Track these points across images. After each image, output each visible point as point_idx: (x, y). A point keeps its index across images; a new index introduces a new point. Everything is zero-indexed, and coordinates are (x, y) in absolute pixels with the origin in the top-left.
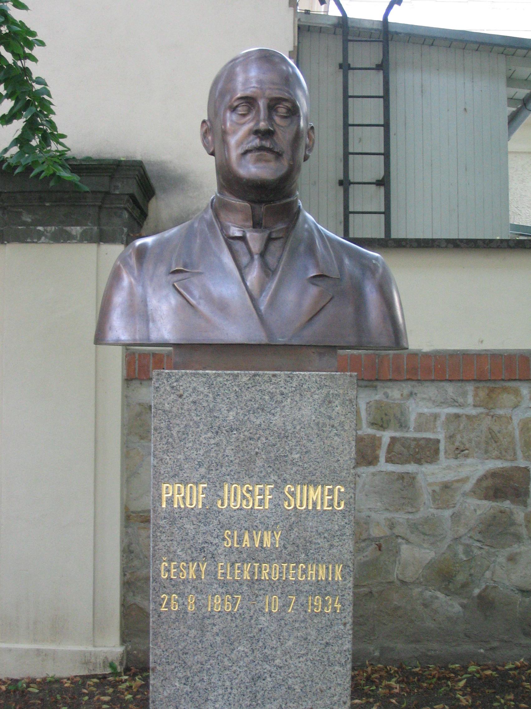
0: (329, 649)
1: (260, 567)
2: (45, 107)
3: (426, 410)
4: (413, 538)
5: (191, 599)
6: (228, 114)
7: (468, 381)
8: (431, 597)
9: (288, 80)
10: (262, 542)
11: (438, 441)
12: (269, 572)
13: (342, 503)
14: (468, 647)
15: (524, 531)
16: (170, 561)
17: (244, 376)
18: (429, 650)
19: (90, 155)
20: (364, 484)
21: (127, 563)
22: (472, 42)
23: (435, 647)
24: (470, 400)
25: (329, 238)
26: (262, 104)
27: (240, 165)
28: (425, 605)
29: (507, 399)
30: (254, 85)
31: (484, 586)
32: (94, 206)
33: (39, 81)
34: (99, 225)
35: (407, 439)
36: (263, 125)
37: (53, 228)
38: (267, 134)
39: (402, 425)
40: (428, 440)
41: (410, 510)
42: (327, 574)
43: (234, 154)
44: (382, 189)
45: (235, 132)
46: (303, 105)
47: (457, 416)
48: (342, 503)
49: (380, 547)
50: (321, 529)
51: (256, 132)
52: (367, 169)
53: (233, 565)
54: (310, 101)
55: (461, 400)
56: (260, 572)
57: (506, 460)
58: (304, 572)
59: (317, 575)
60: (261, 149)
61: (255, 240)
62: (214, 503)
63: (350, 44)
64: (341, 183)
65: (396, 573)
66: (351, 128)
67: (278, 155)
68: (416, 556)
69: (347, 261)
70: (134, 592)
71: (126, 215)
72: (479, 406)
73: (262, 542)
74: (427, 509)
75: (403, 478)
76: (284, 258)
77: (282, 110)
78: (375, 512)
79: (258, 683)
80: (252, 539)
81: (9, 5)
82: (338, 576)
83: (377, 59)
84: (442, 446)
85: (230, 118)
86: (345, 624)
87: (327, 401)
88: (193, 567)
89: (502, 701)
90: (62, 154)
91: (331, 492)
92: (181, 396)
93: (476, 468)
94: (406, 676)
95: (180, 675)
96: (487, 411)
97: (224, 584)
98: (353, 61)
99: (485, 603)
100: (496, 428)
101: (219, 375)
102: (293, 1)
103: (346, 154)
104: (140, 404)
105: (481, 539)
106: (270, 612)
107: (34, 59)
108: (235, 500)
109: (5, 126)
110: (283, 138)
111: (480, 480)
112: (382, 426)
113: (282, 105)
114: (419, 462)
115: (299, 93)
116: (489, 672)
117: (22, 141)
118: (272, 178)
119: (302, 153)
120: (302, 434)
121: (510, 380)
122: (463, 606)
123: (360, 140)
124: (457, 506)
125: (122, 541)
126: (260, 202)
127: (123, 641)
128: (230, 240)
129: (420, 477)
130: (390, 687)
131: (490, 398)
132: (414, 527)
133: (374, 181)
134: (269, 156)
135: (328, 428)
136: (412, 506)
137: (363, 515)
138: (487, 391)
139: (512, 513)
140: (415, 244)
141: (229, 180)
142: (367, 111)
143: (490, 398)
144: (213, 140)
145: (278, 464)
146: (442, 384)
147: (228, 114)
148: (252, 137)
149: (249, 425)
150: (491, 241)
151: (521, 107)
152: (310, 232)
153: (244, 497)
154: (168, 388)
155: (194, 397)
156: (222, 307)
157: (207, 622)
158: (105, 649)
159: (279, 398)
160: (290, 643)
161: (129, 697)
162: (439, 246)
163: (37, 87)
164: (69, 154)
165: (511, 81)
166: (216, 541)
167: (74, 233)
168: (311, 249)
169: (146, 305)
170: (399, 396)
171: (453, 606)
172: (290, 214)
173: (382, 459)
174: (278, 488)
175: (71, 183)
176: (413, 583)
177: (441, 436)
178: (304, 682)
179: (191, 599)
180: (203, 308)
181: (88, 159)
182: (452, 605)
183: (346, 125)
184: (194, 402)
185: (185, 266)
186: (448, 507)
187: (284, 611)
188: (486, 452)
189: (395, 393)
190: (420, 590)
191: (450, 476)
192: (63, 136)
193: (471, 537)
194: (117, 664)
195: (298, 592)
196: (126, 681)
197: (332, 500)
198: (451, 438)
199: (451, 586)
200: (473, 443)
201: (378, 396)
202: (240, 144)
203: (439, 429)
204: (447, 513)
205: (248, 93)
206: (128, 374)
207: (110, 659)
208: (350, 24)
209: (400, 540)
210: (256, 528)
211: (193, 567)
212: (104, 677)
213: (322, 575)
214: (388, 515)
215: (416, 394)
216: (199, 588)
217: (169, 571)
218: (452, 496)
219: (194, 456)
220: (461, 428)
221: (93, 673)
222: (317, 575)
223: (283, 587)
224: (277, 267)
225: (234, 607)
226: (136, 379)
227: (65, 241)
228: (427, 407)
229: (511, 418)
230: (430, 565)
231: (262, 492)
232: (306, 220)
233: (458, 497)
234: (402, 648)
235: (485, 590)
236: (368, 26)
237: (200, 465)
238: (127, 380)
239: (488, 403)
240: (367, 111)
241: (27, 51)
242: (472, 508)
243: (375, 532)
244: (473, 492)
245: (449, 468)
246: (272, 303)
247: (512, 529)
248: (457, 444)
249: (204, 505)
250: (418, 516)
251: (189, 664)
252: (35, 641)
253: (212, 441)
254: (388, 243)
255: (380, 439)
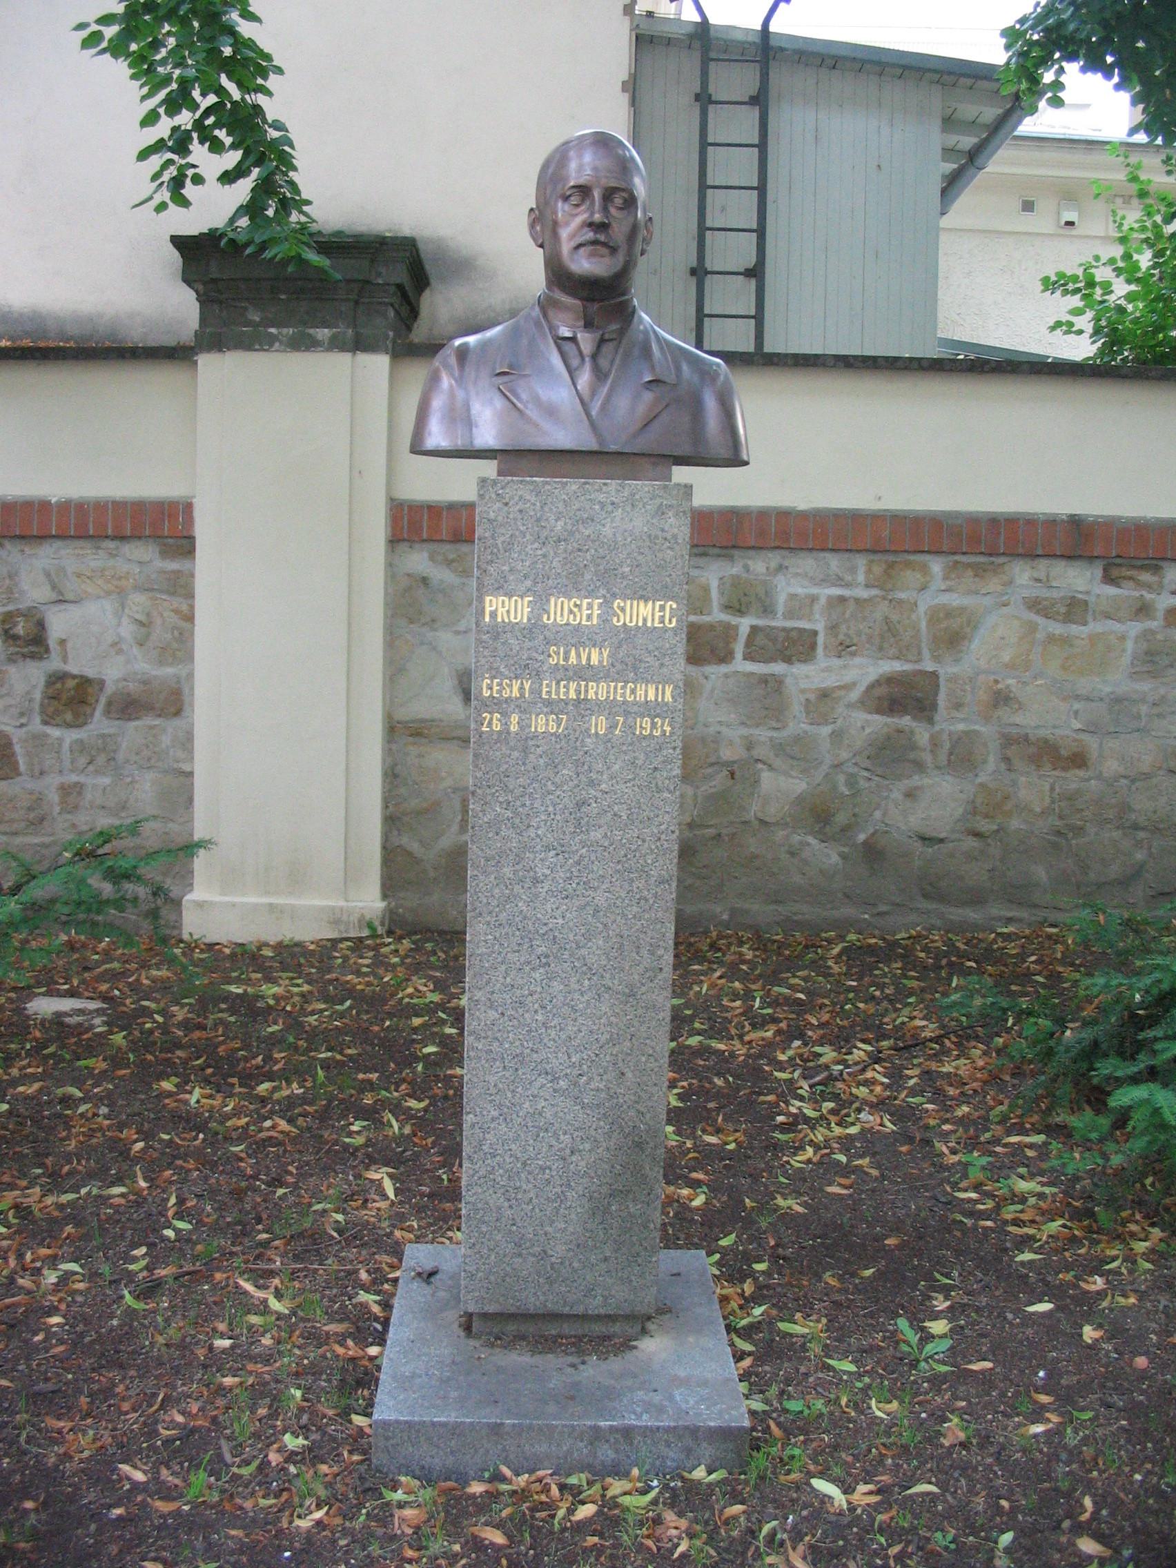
0: (657, 774)
1: (586, 686)
2: (286, 162)
3: (800, 591)
4: (777, 763)
5: (515, 718)
6: (560, 204)
7: (859, 551)
8: (801, 843)
9: (625, 167)
10: (589, 659)
11: (815, 633)
12: (597, 691)
13: (674, 620)
14: (848, 911)
15: (927, 758)
16: (492, 678)
17: (574, 485)
18: (795, 914)
19: (344, 229)
20: (713, 690)
21: (390, 791)
22: (894, 65)
23: (806, 911)
24: (861, 578)
25: (665, 340)
26: (597, 194)
27: (572, 260)
28: (792, 854)
29: (911, 577)
30: (589, 172)
31: (872, 831)
32: (347, 300)
33: (277, 125)
34: (355, 326)
35: (774, 628)
36: (597, 217)
37: (291, 330)
38: (602, 227)
39: (768, 610)
40: (801, 631)
41: (775, 725)
42: (657, 695)
43: (566, 248)
44: (753, 282)
45: (567, 224)
46: (640, 187)
47: (842, 600)
48: (674, 620)
49: (732, 775)
50: (651, 647)
51: (590, 225)
52: (732, 252)
53: (558, 683)
54: (649, 189)
55: (848, 578)
56: (587, 691)
57: (907, 661)
58: (633, 691)
59: (646, 696)
60: (595, 242)
61: (586, 341)
62: (539, 618)
63: (712, 65)
64: (693, 272)
65: (754, 809)
66: (709, 192)
67: (613, 250)
68: (780, 787)
69: (685, 367)
70: (399, 830)
71: (391, 313)
72: (874, 587)
73: (589, 659)
74: (797, 723)
75: (766, 682)
76: (617, 361)
77: (618, 201)
78: (728, 726)
79: (583, 809)
80: (579, 656)
81: (235, 16)
82: (668, 697)
83: (752, 88)
84: (821, 639)
85: (562, 208)
86: (674, 748)
87: (661, 512)
88: (516, 685)
89: (886, 969)
90: (303, 227)
91: (662, 608)
92: (506, 504)
93: (866, 670)
94: (761, 942)
95: (501, 799)
96: (883, 593)
97: (549, 703)
98: (719, 90)
99: (873, 853)
100: (895, 617)
101: (547, 483)
102: (629, 9)
103: (702, 229)
104: (408, 575)
105: (870, 767)
106: (597, 733)
107: (268, 93)
108: (562, 615)
109: (227, 187)
110: (619, 232)
111: (871, 687)
112: (739, 611)
113: (618, 195)
114: (788, 660)
115: (637, 181)
116: (873, 941)
117: (253, 208)
118: (605, 274)
119: (638, 247)
120: (633, 546)
121: (916, 552)
122: (844, 857)
123: (723, 209)
124: (839, 722)
125: (384, 761)
126: (593, 300)
127: (385, 896)
128: (559, 341)
129: (788, 681)
130: (741, 954)
131: (889, 576)
132: (780, 748)
133: (742, 270)
134: (605, 251)
135: (660, 541)
136: (778, 721)
137: (712, 730)
138: (884, 566)
139: (912, 732)
140: (790, 362)
141: (559, 276)
142: (733, 167)
143: (889, 576)
144: (542, 230)
145: (607, 581)
146: (822, 554)
147: (560, 204)
148: (587, 229)
149: (577, 536)
150: (896, 359)
151: (966, 163)
152: (646, 332)
153: (571, 612)
154: (493, 496)
155: (520, 506)
156: (551, 411)
157: (531, 743)
158: (360, 904)
159: (610, 508)
160: (617, 767)
161: (396, 960)
162: (824, 365)
163: (274, 134)
164: (314, 227)
165: (949, 123)
166: (541, 657)
167: (320, 337)
168: (646, 352)
169: (468, 410)
170: (764, 570)
171: (827, 856)
172: (625, 314)
173: (739, 655)
174: (607, 604)
175: (320, 270)
176: (776, 824)
177: (820, 626)
178: (630, 809)
179: (515, 718)
180: (532, 413)
181: (339, 233)
182: (828, 855)
183: (703, 187)
184: (521, 511)
185: (511, 366)
186: (826, 723)
187: (612, 733)
188: (881, 649)
189: (759, 565)
190: (785, 833)
191: (830, 681)
192: (308, 203)
193: (856, 764)
194: (377, 923)
195: (626, 714)
196: (390, 944)
197: (663, 617)
198: (833, 628)
199: (828, 829)
200: (864, 637)
201: (735, 569)
202: (572, 236)
203: (817, 616)
204: (826, 730)
205: (581, 181)
206: (394, 535)
207: (368, 917)
208: (712, 33)
209: (760, 766)
210: (584, 645)
211: (516, 685)
212: (361, 940)
213: (651, 697)
214: (744, 731)
215: (787, 568)
216: (524, 707)
217: (491, 689)
218: (833, 708)
219: (519, 567)
220: (847, 616)
221: (345, 935)
222: (646, 696)
223: (610, 708)
224: (610, 370)
225: (558, 727)
226: (404, 540)
227: (307, 349)
228: (803, 587)
229: (916, 604)
230: (800, 800)
231: (590, 607)
232: (641, 320)
233: (840, 709)
234: (760, 911)
235: (873, 834)
236: (740, 37)
237: (526, 577)
238: (391, 541)
239: (886, 581)
240: (733, 167)
241: (260, 81)
242: (859, 724)
243: (726, 754)
244: (862, 703)
245: (827, 669)
246: (604, 407)
247: (912, 756)
248: (841, 637)
249: (529, 619)
250: (784, 733)
251: (511, 787)
252: (267, 893)
253: (539, 552)
254: (760, 359)
255: (736, 627)
